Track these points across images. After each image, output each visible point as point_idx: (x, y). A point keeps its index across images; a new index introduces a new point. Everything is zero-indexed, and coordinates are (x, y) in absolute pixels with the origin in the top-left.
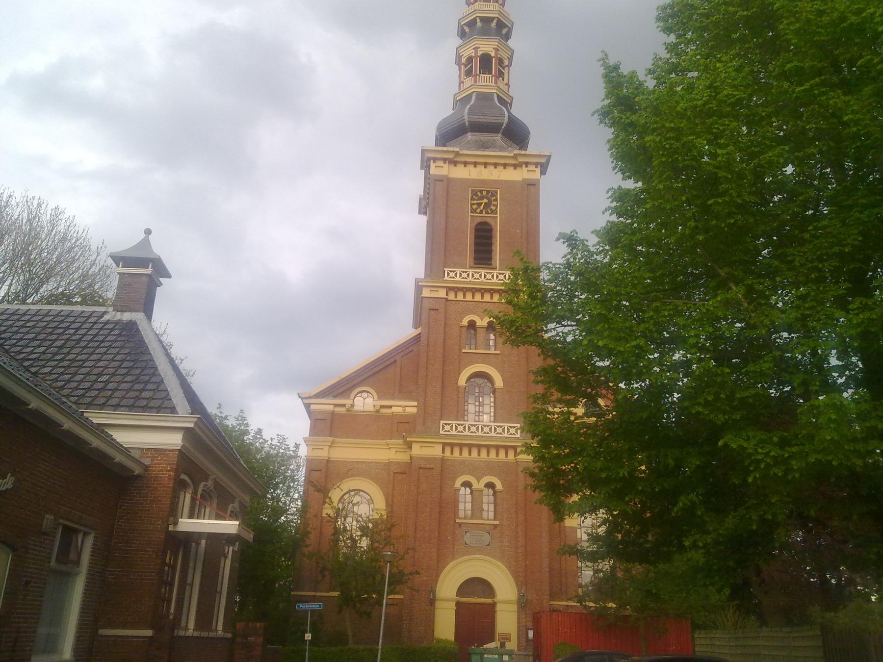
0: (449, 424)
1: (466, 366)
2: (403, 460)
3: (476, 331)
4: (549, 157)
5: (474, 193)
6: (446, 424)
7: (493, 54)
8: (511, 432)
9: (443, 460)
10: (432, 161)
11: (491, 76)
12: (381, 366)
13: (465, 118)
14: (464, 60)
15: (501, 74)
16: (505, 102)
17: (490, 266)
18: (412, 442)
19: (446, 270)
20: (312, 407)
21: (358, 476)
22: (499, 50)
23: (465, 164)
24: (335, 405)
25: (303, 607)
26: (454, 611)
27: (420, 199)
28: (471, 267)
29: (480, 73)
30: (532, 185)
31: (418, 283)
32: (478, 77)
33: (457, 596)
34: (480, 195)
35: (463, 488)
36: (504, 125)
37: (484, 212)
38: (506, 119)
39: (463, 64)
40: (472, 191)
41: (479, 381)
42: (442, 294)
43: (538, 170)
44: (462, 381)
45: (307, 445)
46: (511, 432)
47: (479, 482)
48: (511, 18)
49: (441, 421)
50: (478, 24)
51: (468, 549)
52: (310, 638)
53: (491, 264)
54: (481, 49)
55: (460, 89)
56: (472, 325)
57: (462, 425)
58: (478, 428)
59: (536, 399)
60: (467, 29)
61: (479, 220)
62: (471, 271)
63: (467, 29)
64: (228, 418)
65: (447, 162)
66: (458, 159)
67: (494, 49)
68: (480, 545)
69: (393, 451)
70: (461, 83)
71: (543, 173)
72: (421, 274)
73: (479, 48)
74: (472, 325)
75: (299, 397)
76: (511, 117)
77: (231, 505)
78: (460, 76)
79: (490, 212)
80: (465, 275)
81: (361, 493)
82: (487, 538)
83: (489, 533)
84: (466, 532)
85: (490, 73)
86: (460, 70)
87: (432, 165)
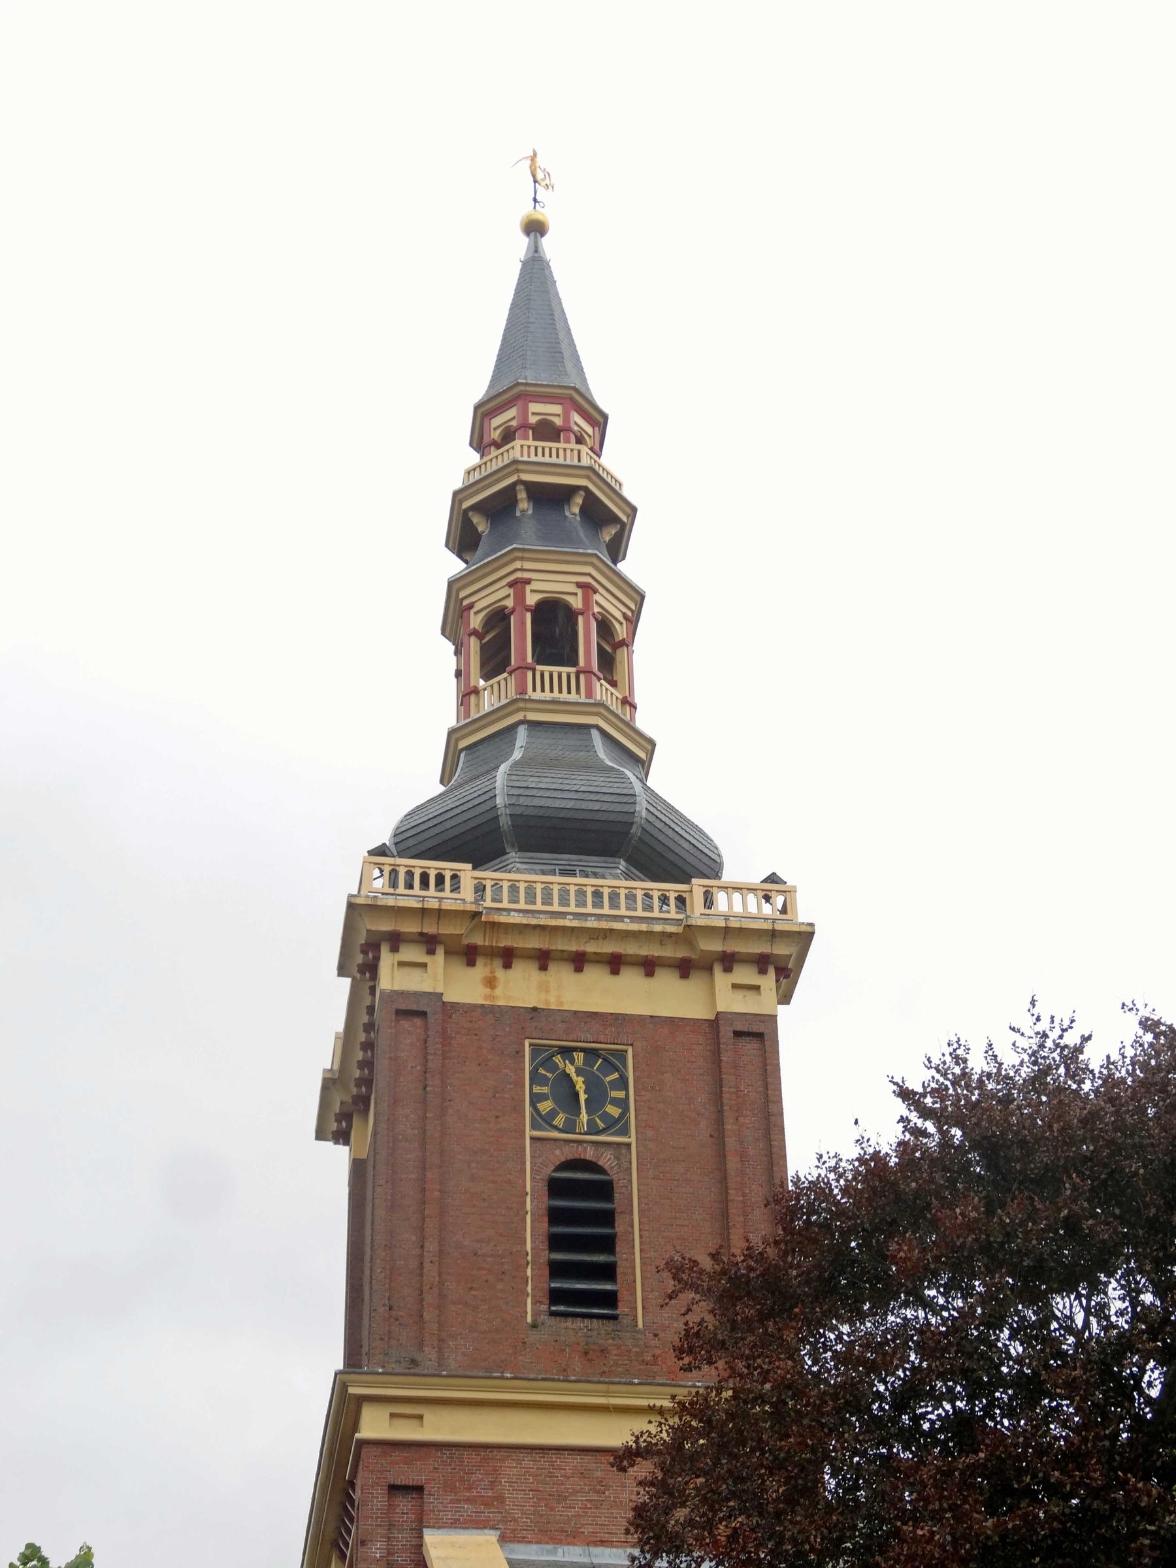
4: (805, 937)
7: (576, 603)
11: (572, 670)
15: (607, 662)
22: (595, 591)
32: (530, 674)
39: (475, 633)
40: (536, 1050)
54: (534, 586)
60: (481, 525)
61: (567, 1153)
63: (481, 525)
65: (440, 951)
66: (478, 940)
67: (579, 585)
70: (467, 695)
87: (387, 960)
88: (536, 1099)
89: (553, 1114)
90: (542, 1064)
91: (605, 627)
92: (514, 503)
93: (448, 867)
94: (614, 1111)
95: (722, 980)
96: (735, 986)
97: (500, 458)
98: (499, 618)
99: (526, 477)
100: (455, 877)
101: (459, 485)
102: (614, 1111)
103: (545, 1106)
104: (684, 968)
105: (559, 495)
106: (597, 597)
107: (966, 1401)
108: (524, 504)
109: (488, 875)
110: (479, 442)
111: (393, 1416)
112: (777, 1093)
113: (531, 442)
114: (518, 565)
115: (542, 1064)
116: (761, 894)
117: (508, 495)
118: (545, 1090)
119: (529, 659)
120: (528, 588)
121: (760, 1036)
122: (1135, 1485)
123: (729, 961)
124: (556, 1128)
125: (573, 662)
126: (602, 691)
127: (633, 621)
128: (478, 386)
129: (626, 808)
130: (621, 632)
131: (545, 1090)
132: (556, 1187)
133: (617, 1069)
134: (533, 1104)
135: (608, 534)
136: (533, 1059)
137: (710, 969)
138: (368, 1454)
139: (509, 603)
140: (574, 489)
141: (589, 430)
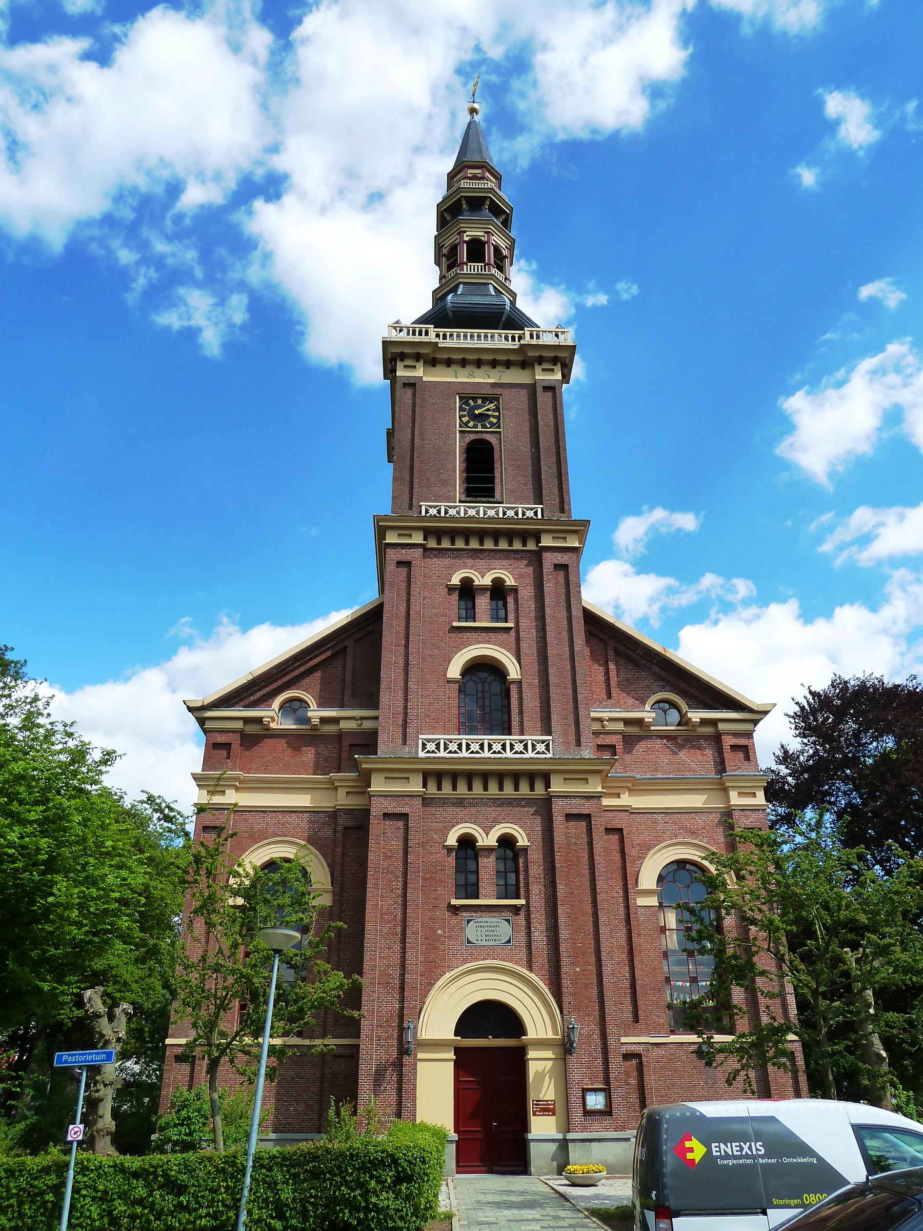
2: (355, 805)
8: (428, 748)
13: (447, 306)
14: (445, 251)
23: (449, 363)
28: (460, 502)
32: (465, 267)
33: (455, 1035)
34: (472, 404)
39: (444, 255)
44: (454, 671)
45: (198, 786)
46: (428, 748)
47: (487, 835)
49: (420, 736)
50: (465, 206)
54: (468, 233)
58: (438, 745)
59: (224, 1120)
61: (473, 437)
64: (780, 753)
67: (486, 232)
68: (493, 943)
69: (341, 793)
72: (386, 509)
73: (465, 232)
79: (489, 426)
87: (400, 365)
88: (460, 417)
89: (468, 422)
90: (463, 404)
91: (497, 249)
94: (495, 421)
95: (538, 369)
96: (543, 370)
98: (454, 249)
103: (465, 419)
107: (616, 303)
111: (399, 535)
112: (833, 1091)
115: (463, 404)
116: (554, 333)
118: (465, 413)
119: (465, 260)
120: (465, 235)
122: (227, 1182)
123: (540, 360)
124: (470, 427)
125: (483, 260)
131: (465, 413)
136: (460, 402)
137: (533, 366)
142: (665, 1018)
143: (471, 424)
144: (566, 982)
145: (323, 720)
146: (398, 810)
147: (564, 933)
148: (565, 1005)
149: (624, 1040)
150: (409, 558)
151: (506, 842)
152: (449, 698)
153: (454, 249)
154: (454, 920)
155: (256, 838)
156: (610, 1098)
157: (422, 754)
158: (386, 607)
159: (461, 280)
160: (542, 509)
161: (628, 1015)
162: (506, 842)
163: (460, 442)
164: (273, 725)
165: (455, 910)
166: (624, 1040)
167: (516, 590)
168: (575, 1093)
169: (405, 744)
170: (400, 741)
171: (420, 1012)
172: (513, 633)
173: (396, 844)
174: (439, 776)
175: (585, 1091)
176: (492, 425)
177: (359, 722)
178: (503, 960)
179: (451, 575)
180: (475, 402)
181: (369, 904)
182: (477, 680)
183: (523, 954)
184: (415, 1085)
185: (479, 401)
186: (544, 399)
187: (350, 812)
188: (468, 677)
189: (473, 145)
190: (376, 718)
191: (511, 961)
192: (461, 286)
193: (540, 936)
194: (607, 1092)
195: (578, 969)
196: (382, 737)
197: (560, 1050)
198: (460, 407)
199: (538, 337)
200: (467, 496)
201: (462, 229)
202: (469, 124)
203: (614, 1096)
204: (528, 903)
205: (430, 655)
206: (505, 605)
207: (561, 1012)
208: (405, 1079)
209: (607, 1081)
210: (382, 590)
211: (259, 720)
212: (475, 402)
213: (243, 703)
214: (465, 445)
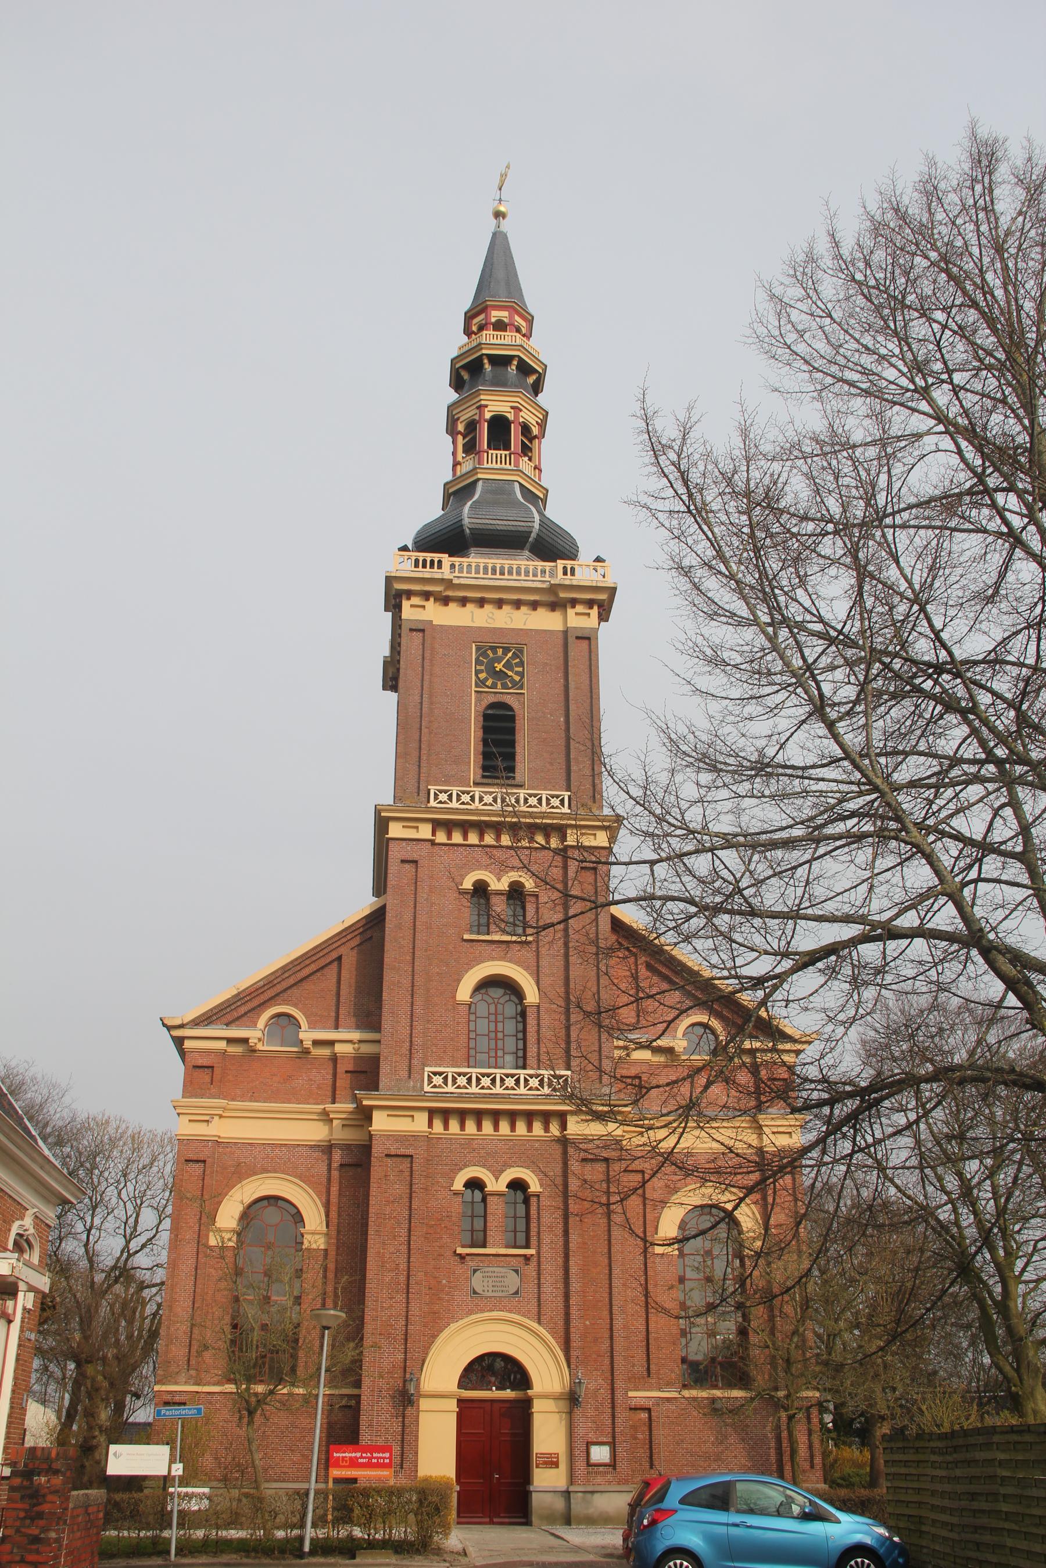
0: (440, 1074)
1: (470, 966)
3: (488, 900)
4: (612, 591)
5: (482, 651)
6: (435, 1074)
7: (511, 417)
9: (428, 1139)
10: (404, 597)
11: (507, 452)
12: (313, 967)
15: (526, 450)
16: (536, 498)
17: (509, 782)
18: (371, 1108)
19: (433, 789)
20: (188, 1044)
21: (427, 1354)
22: (521, 410)
23: (463, 601)
24: (230, 1041)
25: (168, 1413)
26: (453, 1418)
27: (385, 663)
28: (476, 784)
29: (489, 447)
30: (588, 638)
31: (380, 814)
33: (461, 1385)
34: (491, 655)
35: (469, 1191)
36: (533, 535)
37: (499, 686)
38: (536, 526)
40: (478, 649)
41: (497, 993)
42: (425, 831)
43: (594, 612)
44: (464, 992)
47: (497, 1179)
48: (531, 310)
49: (427, 1069)
51: (479, 1302)
52: (180, 1472)
53: (514, 778)
54: (489, 408)
55: (454, 474)
56: (481, 889)
57: (465, 1074)
60: (466, 376)
61: (492, 699)
62: (477, 791)
63: (466, 376)
65: (432, 599)
66: (450, 593)
67: (512, 408)
68: (500, 1294)
70: (456, 464)
71: (604, 617)
72: (386, 797)
73: (486, 406)
74: (481, 889)
75: (164, 1025)
76: (545, 522)
77: (17, 1223)
78: (454, 454)
80: (466, 798)
81: (280, 1203)
82: (513, 1281)
83: (516, 1271)
84: (475, 1271)
85: (507, 447)
86: (454, 442)
87: (406, 604)
88: (477, 672)
89: (486, 679)
90: (481, 655)
91: (526, 429)
92: (482, 365)
93: (436, 556)
96: (576, 614)
97: (475, 341)
99: (484, 352)
100: (440, 562)
101: (455, 354)
102: (489, 683)
103: (482, 676)
104: (553, 606)
105: (500, 361)
106: (522, 414)
108: (487, 367)
109: (457, 560)
110: (468, 332)
113: (492, 332)
114: (518, 399)
115: (481, 655)
117: (478, 362)
118: (483, 668)
121: (589, 639)
123: (574, 602)
124: (488, 687)
126: (525, 465)
127: (546, 496)
128: (467, 304)
129: (530, 524)
130: (535, 431)
131: (483, 668)
132: (486, 717)
133: (518, 657)
134: (476, 675)
135: (531, 380)
138: (391, 844)
139: (477, 417)
140: (512, 357)
141: (524, 324)
142: (677, 1370)
143: (489, 683)
144: (575, 1336)
145: (316, 1043)
146: (402, 1151)
147: (575, 1286)
148: (573, 1360)
149: (631, 1394)
150: (415, 856)
151: (516, 892)
152: (458, 1023)
153: (472, 426)
154: (459, 1269)
155: (241, 1173)
156: (615, 1451)
157: (427, 1088)
158: (389, 916)
159: (480, 476)
160: (569, 797)
161: (640, 1369)
162: (518, 1185)
163: (476, 706)
164: (260, 1047)
165: (462, 1257)
166: (631, 1394)
167: (537, 896)
168: (580, 1447)
169: (410, 1077)
170: (404, 1074)
171: (423, 1364)
172: (534, 945)
173: (399, 1189)
174: (446, 1114)
175: (589, 1444)
176: (515, 684)
177: (356, 1045)
178: (510, 1311)
179: (463, 877)
180: (495, 652)
181: (371, 1253)
182: (490, 1001)
183: (535, 1310)
184: (417, 1437)
185: (500, 652)
186: (577, 650)
187: (347, 1147)
188: (479, 997)
189: (500, 274)
190: (379, 1042)
191: (519, 1314)
192: (480, 483)
193: (552, 1289)
194: (613, 1445)
195: (587, 1323)
196: (384, 1069)
197: (563, 1405)
198: (477, 660)
199: (573, 573)
200: (484, 777)
201: (483, 402)
202: (494, 234)
203: (619, 1449)
204: (538, 1253)
205: (438, 973)
206: (524, 908)
207: (569, 1366)
208: (407, 1430)
209: (614, 1437)
210: (380, 887)
211: (245, 1041)
212: (495, 652)
213: (225, 1020)
214: (481, 709)
